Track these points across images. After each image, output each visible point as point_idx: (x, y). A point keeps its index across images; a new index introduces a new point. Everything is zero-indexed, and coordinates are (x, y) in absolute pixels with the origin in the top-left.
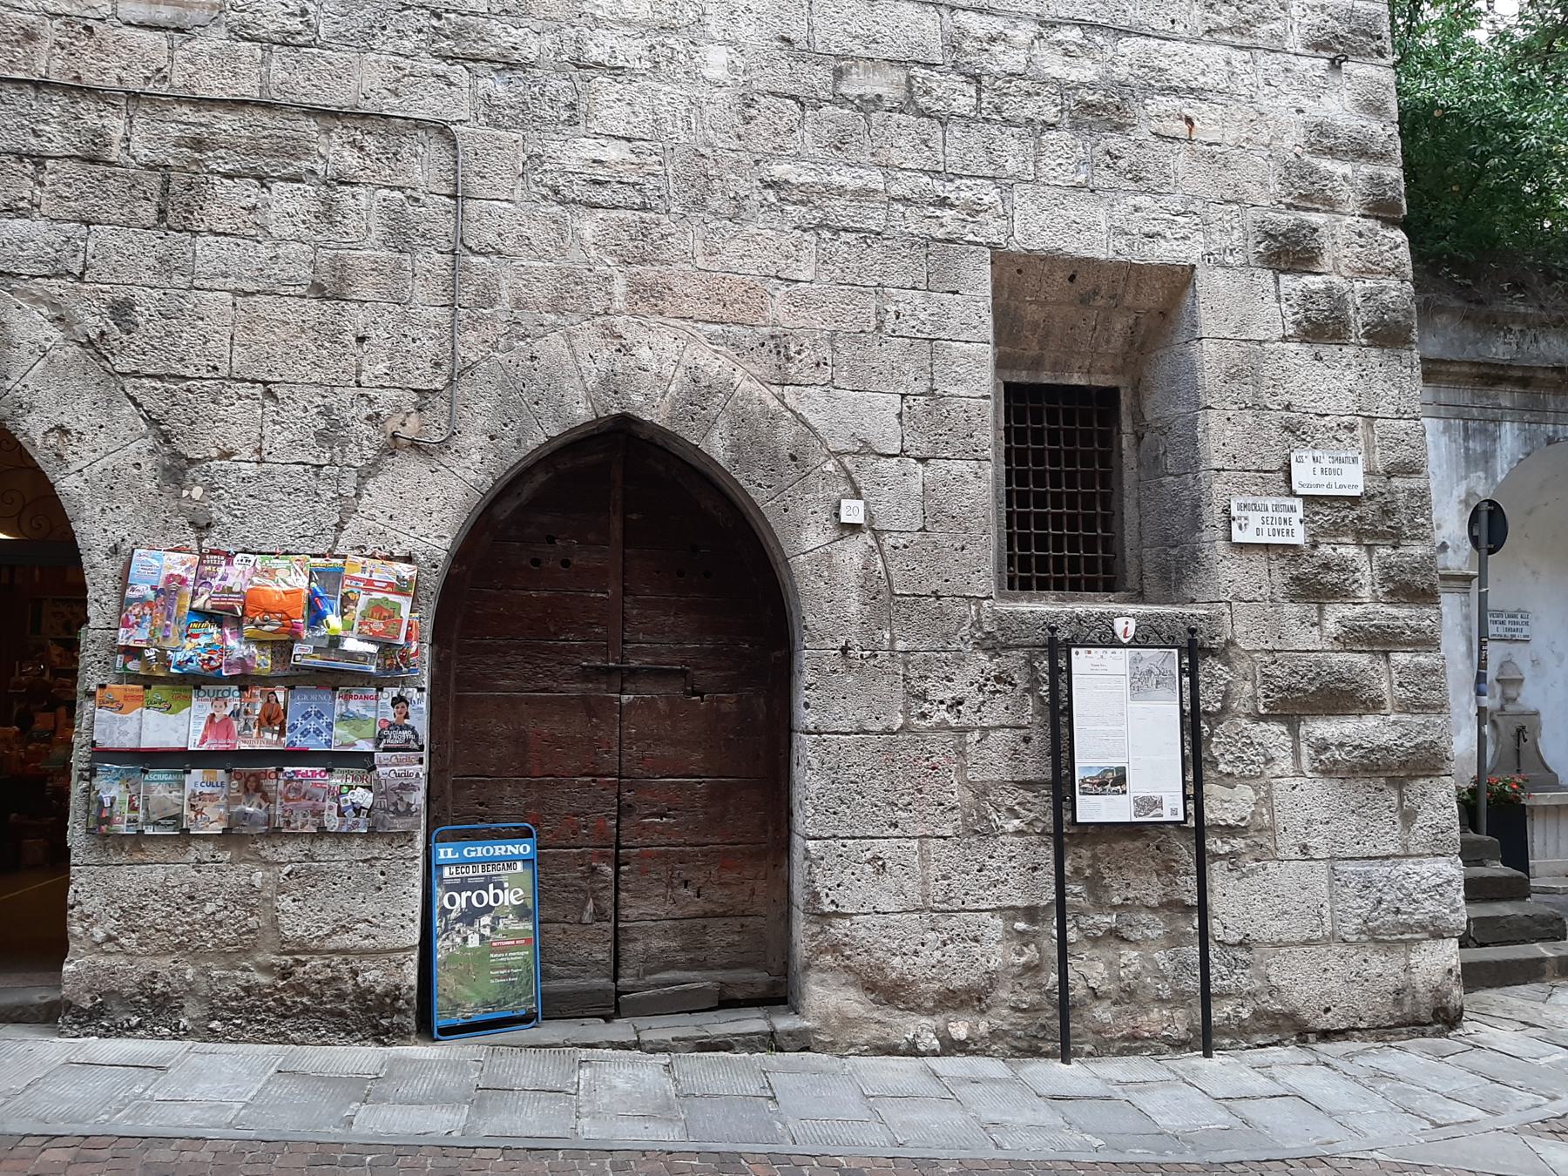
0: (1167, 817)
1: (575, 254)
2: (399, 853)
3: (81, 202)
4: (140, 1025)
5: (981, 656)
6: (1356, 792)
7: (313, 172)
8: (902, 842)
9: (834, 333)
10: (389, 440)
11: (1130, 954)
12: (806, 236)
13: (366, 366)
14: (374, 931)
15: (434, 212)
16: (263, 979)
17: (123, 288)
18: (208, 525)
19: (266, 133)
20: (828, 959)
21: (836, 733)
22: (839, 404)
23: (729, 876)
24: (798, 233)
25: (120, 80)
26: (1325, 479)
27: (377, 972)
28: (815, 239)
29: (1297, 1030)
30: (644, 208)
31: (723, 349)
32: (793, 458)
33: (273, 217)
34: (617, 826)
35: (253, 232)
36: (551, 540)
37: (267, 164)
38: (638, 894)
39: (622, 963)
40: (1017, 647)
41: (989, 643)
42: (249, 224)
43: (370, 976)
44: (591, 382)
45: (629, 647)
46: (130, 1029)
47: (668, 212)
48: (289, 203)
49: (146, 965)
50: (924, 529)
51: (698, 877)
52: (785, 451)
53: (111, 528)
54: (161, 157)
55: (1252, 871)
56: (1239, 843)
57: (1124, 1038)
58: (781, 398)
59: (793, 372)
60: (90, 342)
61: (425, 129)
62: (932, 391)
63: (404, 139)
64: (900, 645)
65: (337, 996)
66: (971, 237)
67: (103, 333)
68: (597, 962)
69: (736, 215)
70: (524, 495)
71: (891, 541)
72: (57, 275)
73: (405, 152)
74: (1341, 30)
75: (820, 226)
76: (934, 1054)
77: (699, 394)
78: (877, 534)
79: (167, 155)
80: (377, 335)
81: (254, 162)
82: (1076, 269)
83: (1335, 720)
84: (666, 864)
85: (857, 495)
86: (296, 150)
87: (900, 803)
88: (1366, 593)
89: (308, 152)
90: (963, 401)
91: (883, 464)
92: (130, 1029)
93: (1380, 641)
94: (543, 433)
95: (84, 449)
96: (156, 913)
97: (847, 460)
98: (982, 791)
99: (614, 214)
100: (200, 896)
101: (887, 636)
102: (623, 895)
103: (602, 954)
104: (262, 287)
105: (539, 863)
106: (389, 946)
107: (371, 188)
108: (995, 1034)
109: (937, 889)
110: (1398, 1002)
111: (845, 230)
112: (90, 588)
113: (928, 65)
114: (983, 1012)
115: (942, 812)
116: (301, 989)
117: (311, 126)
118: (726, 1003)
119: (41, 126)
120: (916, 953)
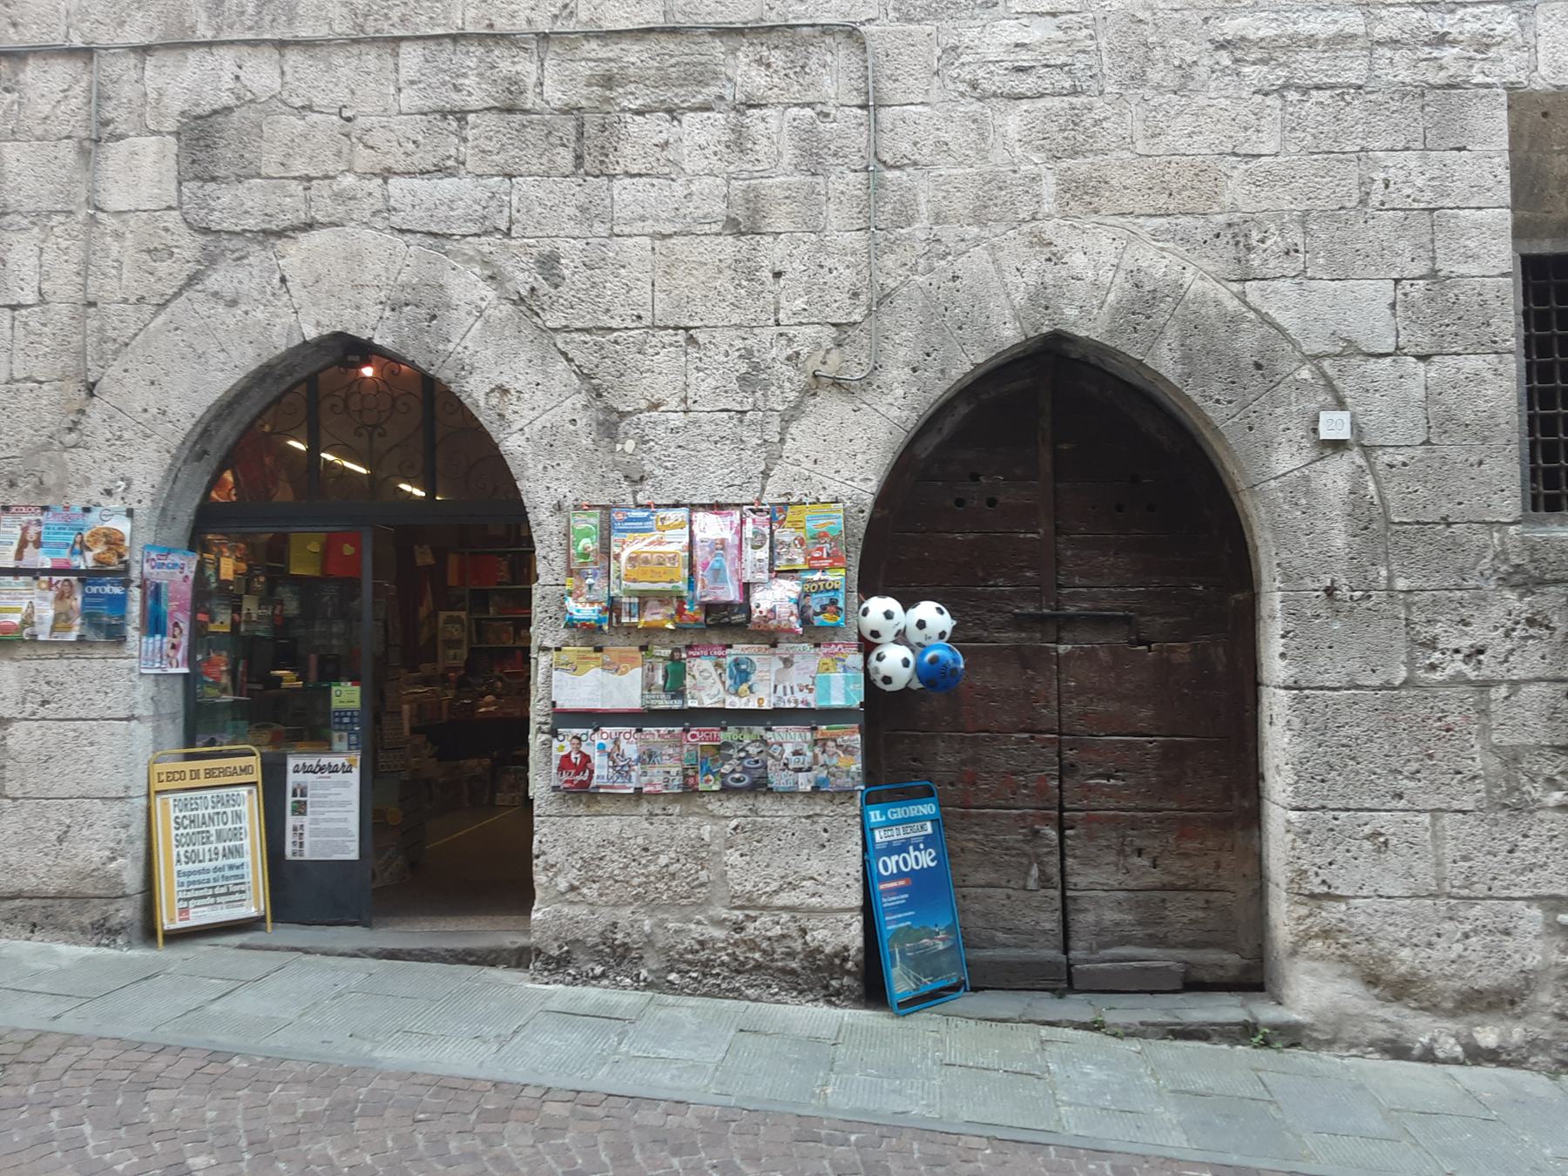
1: (998, 156)
2: (840, 810)
3: (503, 155)
4: (604, 975)
5: (1508, 594)
7: (721, 98)
8: (1409, 817)
9: (1307, 212)
10: (810, 380)
12: (1269, 101)
13: (783, 303)
14: (821, 889)
15: (847, 124)
16: (719, 933)
17: (548, 241)
18: (642, 478)
19: (673, 61)
20: (1318, 945)
21: (1321, 688)
22: (1315, 297)
23: (1191, 845)
24: (1259, 98)
25: (529, 22)
27: (825, 932)
28: (1278, 103)
30: (1075, 92)
31: (1170, 245)
32: (1258, 366)
33: (686, 152)
34: (1060, 787)
35: (667, 170)
36: (975, 478)
37: (676, 95)
38: (1087, 861)
39: (1073, 934)
40: (1556, 582)
41: (1517, 578)
42: (662, 161)
43: (820, 935)
44: (1019, 298)
45: (1065, 591)
46: (595, 978)
47: (1101, 93)
48: (700, 133)
49: (605, 916)
50: (1427, 442)
51: (1154, 845)
52: (1248, 360)
53: (553, 485)
54: (574, 100)
58: (1242, 297)
59: (1256, 263)
60: (522, 299)
61: (833, 34)
62: (1433, 274)
63: (811, 49)
64: (1401, 584)
65: (788, 954)
66: (1480, 79)
67: (533, 289)
68: (1045, 932)
69: (1183, 86)
70: (945, 432)
71: (1386, 459)
72: (486, 233)
73: (813, 63)
75: (1286, 87)
76: (1455, 1061)
77: (1144, 301)
78: (1367, 450)
79: (580, 95)
80: (794, 268)
81: (667, 94)
84: (1115, 829)
85: (1341, 404)
86: (701, 76)
87: (1407, 770)
89: (716, 75)
90: (1476, 282)
91: (1372, 364)
92: (595, 978)
94: (965, 361)
95: (523, 408)
96: (613, 864)
97: (1326, 364)
98: (1512, 757)
99: (1040, 103)
100: (653, 848)
101: (1384, 573)
102: (1069, 861)
103: (1050, 922)
104: (679, 227)
106: (836, 906)
107: (780, 108)
108: (1533, 1044)
109: (1455, 873)
111: (1318, 88)
112: (538, 545)
114: (1518, 1017)
115: (1461, 782)
116: (753, 945)
117: (718, 47)
118: (1193, 984)
119: (461, 81)
120: (1430, 945)
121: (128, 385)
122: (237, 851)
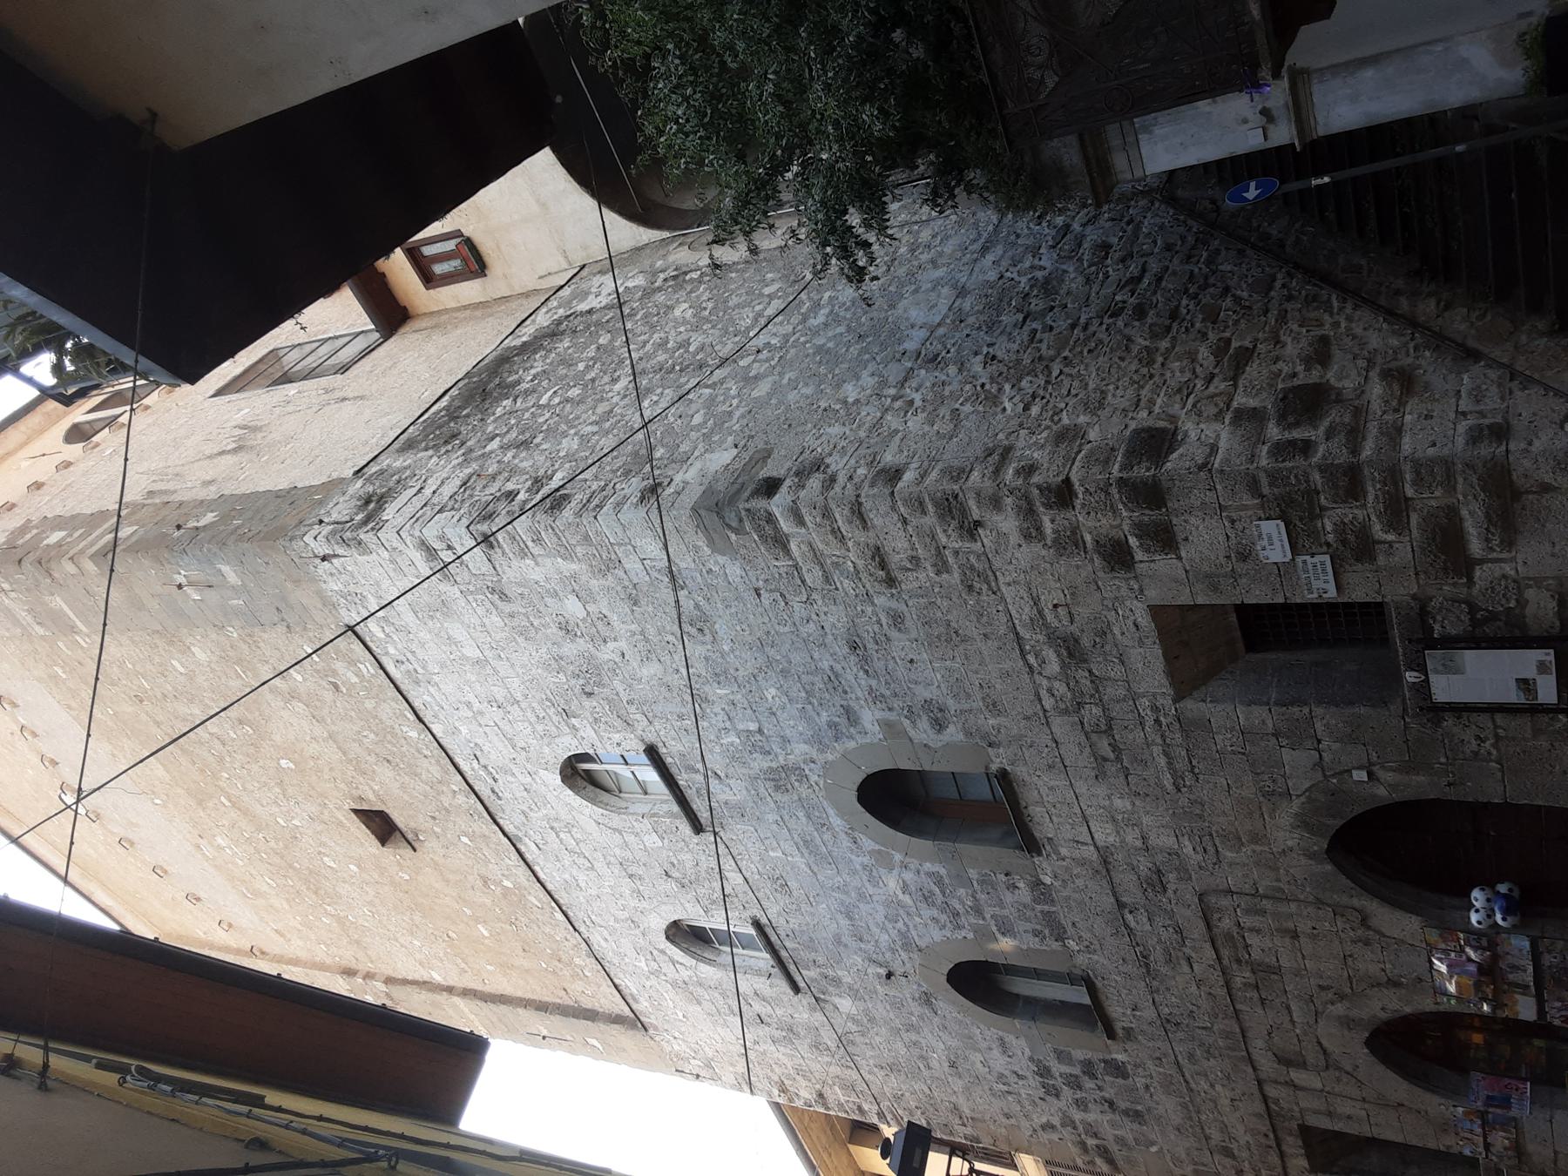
0: (1552, 658)
26: (1277, 544)
64: (1443, 760)
74: (954, 524)
77: (1304, 822)
82: (1170, 659)
85: (1349, 771)
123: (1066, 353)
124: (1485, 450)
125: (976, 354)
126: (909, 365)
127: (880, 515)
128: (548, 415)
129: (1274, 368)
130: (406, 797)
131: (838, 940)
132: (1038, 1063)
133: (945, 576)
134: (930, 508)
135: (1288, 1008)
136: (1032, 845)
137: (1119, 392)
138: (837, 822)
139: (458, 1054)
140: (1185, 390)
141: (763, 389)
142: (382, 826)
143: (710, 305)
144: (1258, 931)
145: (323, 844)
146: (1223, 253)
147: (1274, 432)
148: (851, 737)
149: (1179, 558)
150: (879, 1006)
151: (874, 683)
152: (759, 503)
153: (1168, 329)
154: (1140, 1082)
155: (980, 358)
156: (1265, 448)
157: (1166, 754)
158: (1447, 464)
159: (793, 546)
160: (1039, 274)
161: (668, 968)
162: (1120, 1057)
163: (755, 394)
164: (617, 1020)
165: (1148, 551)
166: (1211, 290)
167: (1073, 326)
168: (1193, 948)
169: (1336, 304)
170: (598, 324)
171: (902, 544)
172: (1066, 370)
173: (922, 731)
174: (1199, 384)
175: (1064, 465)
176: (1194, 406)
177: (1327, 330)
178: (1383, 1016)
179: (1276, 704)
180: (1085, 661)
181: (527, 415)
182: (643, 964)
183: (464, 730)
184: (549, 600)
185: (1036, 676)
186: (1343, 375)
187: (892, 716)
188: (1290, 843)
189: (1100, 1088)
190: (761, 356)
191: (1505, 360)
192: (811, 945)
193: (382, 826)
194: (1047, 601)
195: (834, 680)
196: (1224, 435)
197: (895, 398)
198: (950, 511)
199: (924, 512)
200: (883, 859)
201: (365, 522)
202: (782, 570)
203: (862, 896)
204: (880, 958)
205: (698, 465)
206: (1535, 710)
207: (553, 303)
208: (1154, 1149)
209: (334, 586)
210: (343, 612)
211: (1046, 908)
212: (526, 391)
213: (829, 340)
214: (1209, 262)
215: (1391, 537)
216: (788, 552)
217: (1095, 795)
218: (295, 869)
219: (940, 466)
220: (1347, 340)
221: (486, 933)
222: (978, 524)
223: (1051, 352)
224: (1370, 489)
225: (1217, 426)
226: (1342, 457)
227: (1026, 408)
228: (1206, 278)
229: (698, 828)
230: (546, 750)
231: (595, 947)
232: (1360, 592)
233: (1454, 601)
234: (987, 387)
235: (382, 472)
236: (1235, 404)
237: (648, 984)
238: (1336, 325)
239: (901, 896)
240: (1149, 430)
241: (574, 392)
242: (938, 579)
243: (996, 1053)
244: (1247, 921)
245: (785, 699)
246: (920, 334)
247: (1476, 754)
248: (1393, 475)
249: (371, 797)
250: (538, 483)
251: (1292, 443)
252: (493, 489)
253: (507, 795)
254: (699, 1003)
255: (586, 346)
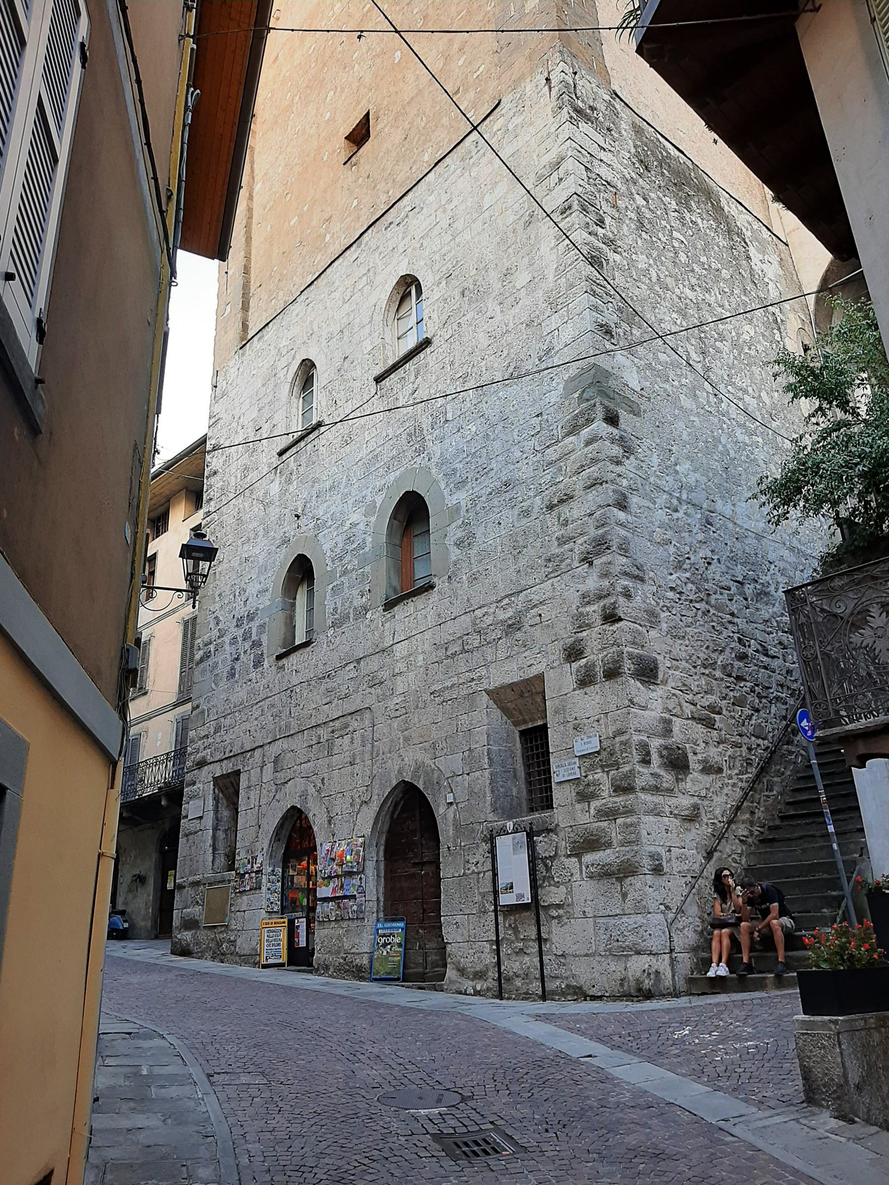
6: (605, 885)
11: (527, 959)
29: (580, 994)
55: (565, 923)
56: (561, 912)
57: (525, 993)
64: (463, 844)
74: (590, 548)
77: (419, 767)
82: (512, 686)
83: (594, 853)
88: (605, 794)
93: (609, 814)
105: (406, 930)
108: (488, 989)
110: (622, 985)
113: (468, 634)
121: (264, 826)
122: (279, 945)
123: (712, 611)
124: (646, 863)
125: (712, 551)
126: (705, 506)
127: (594, 498)
128: (664, 239)
129: (700, 742)
130: (381, 154)
131: (315, 481)
132: (255, 614)
133: (556, 543)
134: (601, 531)
135: (309, 761)
136: (389, 605)
137: (683, 648)
138: (392, 477)
139: (218, 249)
140: (685, 688)
141: (686, 402)
142: (360, 135)
143: (753, 353)
144: (352, 742)
145: (342, 91)
146: (784, 707)
147: (655, 743)
148: (447, 485)
149: (574, 690)
150: (278, 510)
151: (484, 499)
152: (600, 413)
153: (730, 676)
154: (253, 676)
155: (709, 554)
156: (645, 738)
157: (453, 685)
158: (637, 841)
159: (571, 439)
160: (772, 589)
161: (283, 362)
162: (266, 664)
163: (682, 397)
164: (245, 327)
165: (578, 671)
166: (757, 701)
167: (732, 614)
168: (337, 705)
169: (745, 777)
170: (738, 266)
171: (576, 513)
172: (700, 612)
173: (455, 533)
174: (690, 697)
175: (631, 617)
176: (674, 695)
177: (726, 771)
178: (310, 816)
179: (488, 749)
180: (507, 635)
181: (664, 223)
182: (284, 343)
183: (431, 198)
184: (526, 260)
185: (495, 605)
186: (695, 781)
187: (463, 512)
188: (406, 759)
189: (245, 652)
190: (711, 397)
191: (705, 873)
192: (311, 463)
193: (360, 135)
194: (543, 609)
195: (485, 471)
196: (653, 714)
197: (679, 499)
198: (599, 545)
199: (597, 527)
200: (371, 509)
201: (578, 111)
202: (555, 431)
203: (345, 496)
204: (307, 510)
205: (628, 363)
206: (496, 893)
207: (756, 225)
208: (213, 685)
209: (529, 87)
210: (510, 97)
211: (351, 616)
212: (683, 218)
213: (724, 446)
214: (777, 698)
215: (592, 812)
216: (568, 434)
217: (425, 643)
218: (323, 68)
219: (629, 535)
220: (719, 784)
221: (292, 223)
222: (591, 564)
223: (713, 602)
224: (621, 799)
225: (660, 709)
226: (639, 782)
227: (672, 589)
228: (766, 697)
229: (378, 379)
230: (422, 263)
231: (291, 307)
232: (560, 795)
233: (556, 847)
234: (687, 561)
235: (617, 115)
236: (674, 719)
237: (272, 348)
238: (730, 777)
239: (348, 522)
240: (656, 668)
241: (683, 257)
242: (554, 539)
243: (258, 587)
244: (357, 735)
245: (469, 438)
246: (728, 510)
247: (468, 862)
248: (629, 812)
249: (379, 127)
250: (609, 242)
251: (648, 754)
252: (606, 207)
253: (389, 235)
254: (263, 385)
255: (720, 260)
